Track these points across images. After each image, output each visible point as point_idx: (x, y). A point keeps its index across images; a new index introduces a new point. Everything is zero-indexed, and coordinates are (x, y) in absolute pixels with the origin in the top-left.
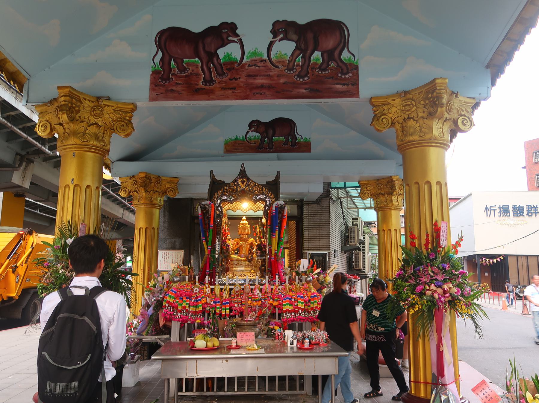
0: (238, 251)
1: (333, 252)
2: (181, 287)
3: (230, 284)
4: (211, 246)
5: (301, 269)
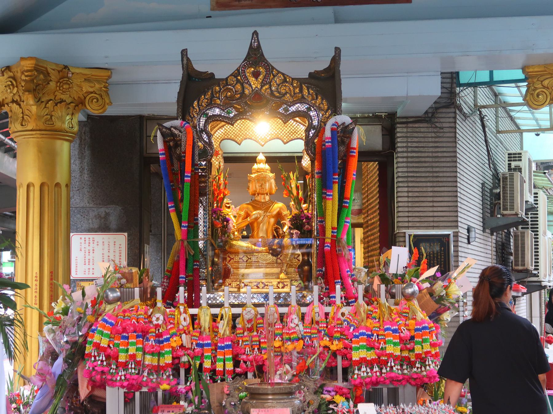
1: (465, 232)
2: (124, 311)
3: (233, 306)
4: (189, 222)
5: (392, 270)
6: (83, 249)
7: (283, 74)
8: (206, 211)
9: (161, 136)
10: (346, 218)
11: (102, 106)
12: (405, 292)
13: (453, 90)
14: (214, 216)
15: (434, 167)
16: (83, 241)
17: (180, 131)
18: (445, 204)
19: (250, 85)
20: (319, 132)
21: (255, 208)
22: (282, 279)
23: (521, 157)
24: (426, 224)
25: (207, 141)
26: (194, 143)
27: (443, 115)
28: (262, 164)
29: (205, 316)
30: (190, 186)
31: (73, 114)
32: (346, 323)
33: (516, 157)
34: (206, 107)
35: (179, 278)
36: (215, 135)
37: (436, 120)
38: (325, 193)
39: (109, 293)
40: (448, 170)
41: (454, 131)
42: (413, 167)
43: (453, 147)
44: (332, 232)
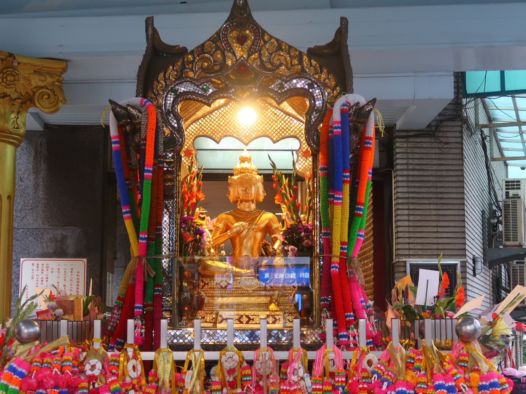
0: (231, 247)
1: (471, 262)
2: (43, 355)
3: (206, 347)
4: (149, 233)
5: (420, 300)
6: (35, 277)
7: (277, 40)
8: (173, 219)
9: (115, 119)
10: (360, 230)
11: (54, 103)
12: (461, 330)
13: (459, 100)
14: (183, 226)
15: (438, 187)
16: (35, 267)
17: (140, 112)
18: (451, 230)
19: (234, 54)
20: (324, 115)
21: (238, 219)
22: (272, 311)
23: (520, 185)
24: (429, 252)
25: (176, 125)
26: (157, 127)
27: (449, 129)
28: (246, 162)
29: (164, 361)
30: (152, 184)
31: (18, 113)
32: (375, 375)
33: (514, 185)
34: (175, 82)
35: (134, 308)
36: (188, 130)
37: (441, 134)
38: (333, 196)
39: (23, 327)
40: (454, 190)
41: (460, 146)
42: (415, 187)
43: (459, 165)
44: (342, 248)
